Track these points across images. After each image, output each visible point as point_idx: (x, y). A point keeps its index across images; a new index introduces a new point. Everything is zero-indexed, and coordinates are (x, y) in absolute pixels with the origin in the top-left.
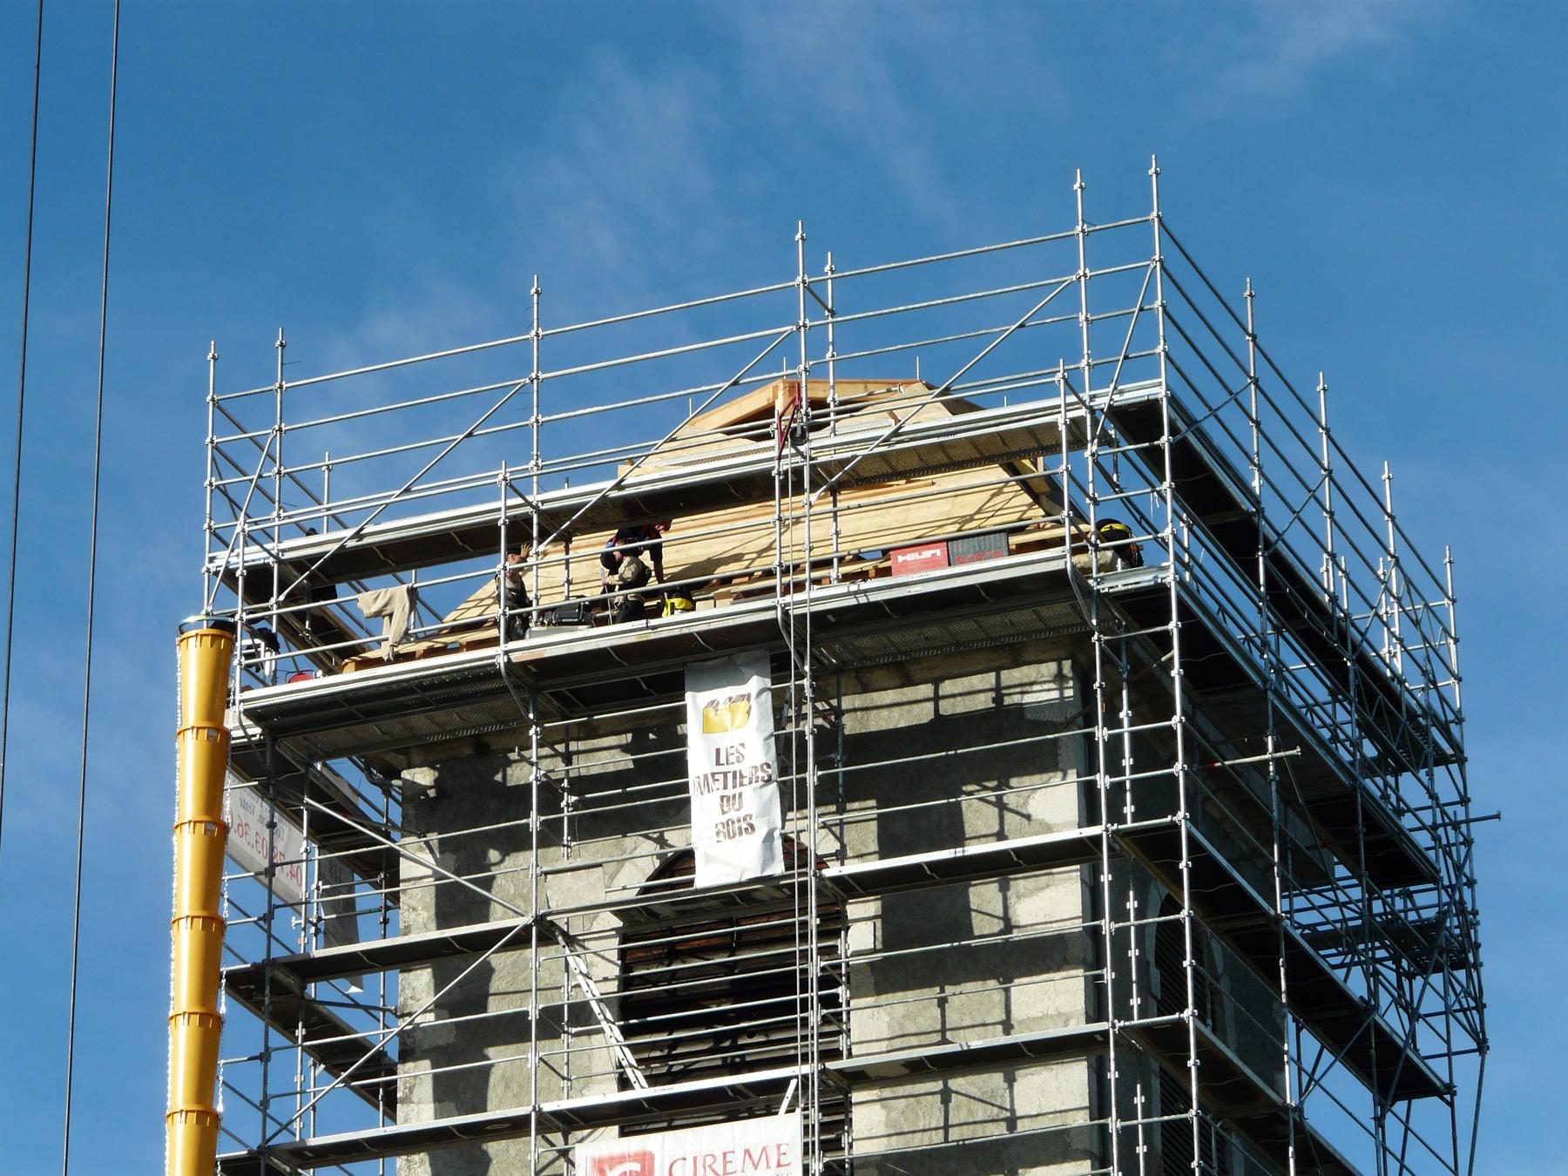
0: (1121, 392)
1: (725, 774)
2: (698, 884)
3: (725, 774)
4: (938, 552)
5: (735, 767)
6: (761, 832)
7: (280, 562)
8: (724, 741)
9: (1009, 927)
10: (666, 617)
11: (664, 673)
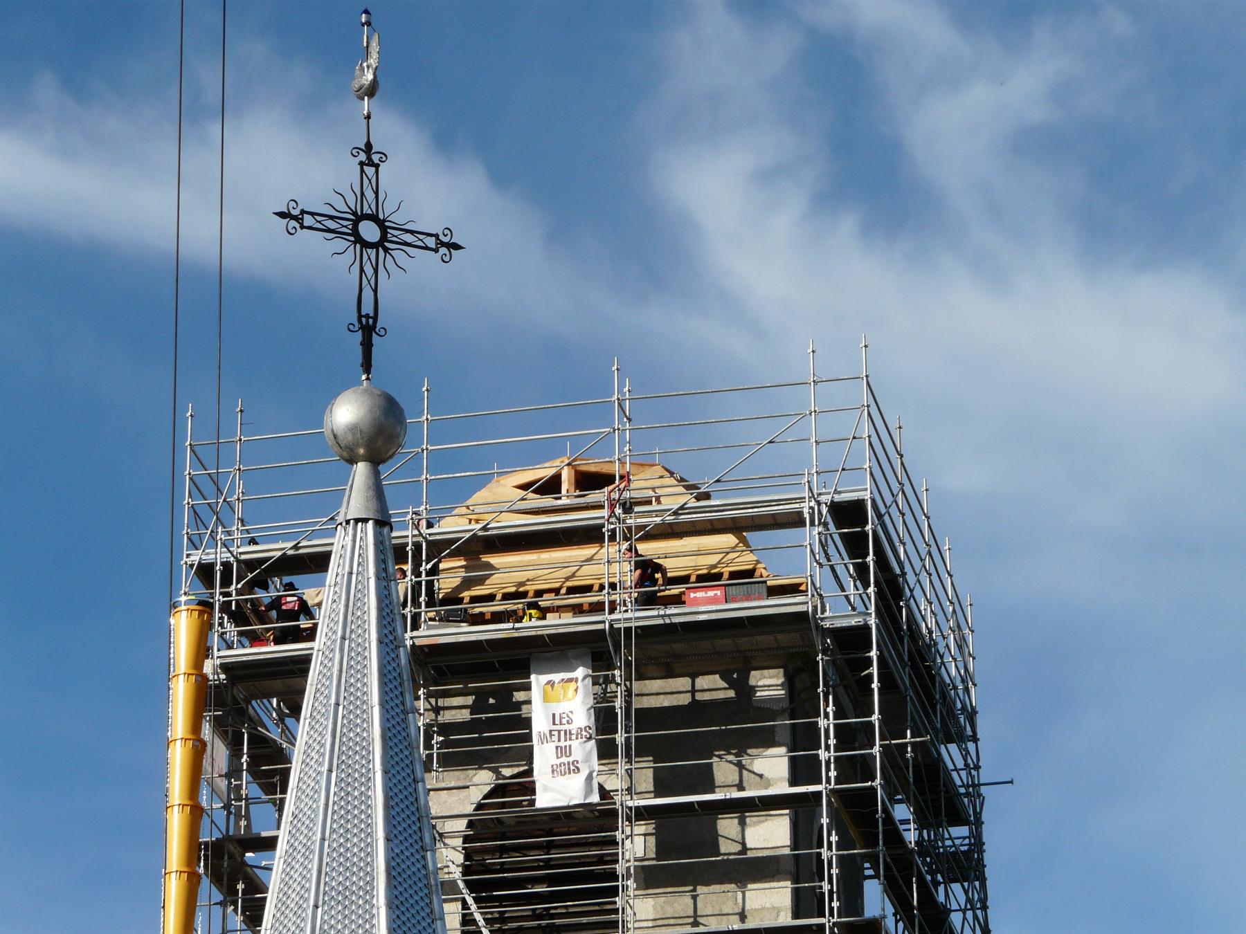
0: (840, 493)
1: (559, 731)
2: (539, 805)
3: (559, 731)
4: (719, 593)
5: (567, 727)
6: (584, 773)
7: (238, 561)
8: (561, 708)
9: (745, 849)
10: (526, 622)
11: (521, 658)
